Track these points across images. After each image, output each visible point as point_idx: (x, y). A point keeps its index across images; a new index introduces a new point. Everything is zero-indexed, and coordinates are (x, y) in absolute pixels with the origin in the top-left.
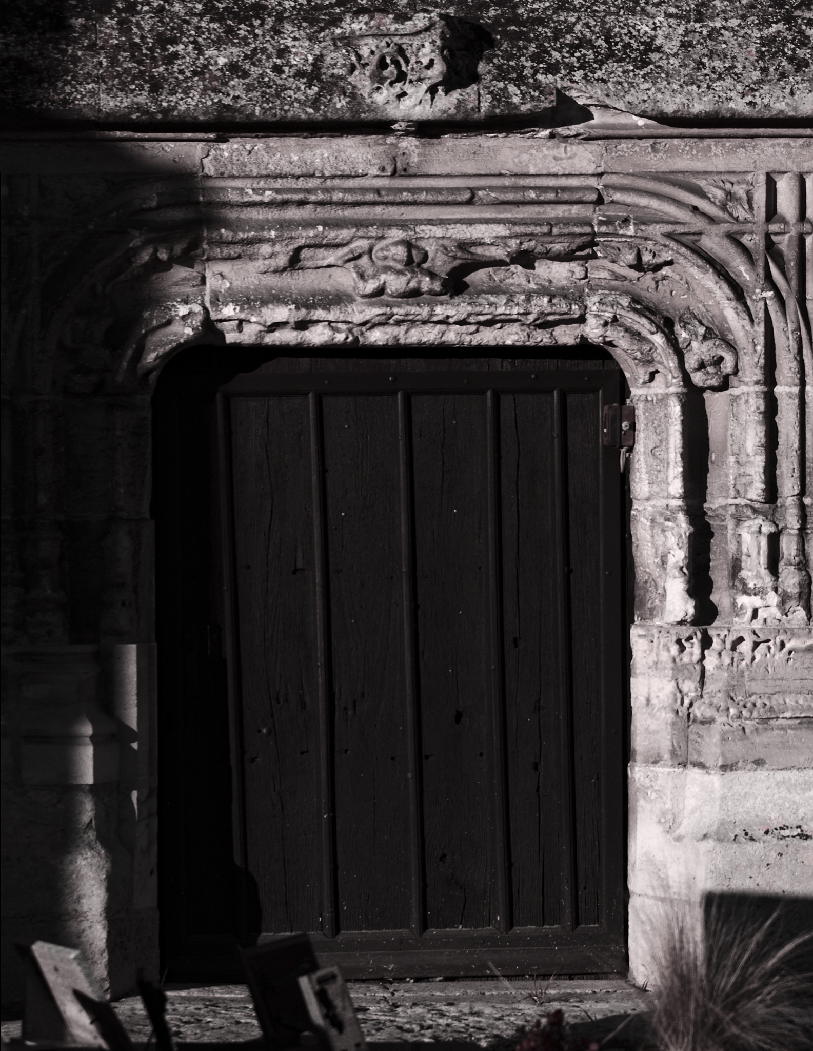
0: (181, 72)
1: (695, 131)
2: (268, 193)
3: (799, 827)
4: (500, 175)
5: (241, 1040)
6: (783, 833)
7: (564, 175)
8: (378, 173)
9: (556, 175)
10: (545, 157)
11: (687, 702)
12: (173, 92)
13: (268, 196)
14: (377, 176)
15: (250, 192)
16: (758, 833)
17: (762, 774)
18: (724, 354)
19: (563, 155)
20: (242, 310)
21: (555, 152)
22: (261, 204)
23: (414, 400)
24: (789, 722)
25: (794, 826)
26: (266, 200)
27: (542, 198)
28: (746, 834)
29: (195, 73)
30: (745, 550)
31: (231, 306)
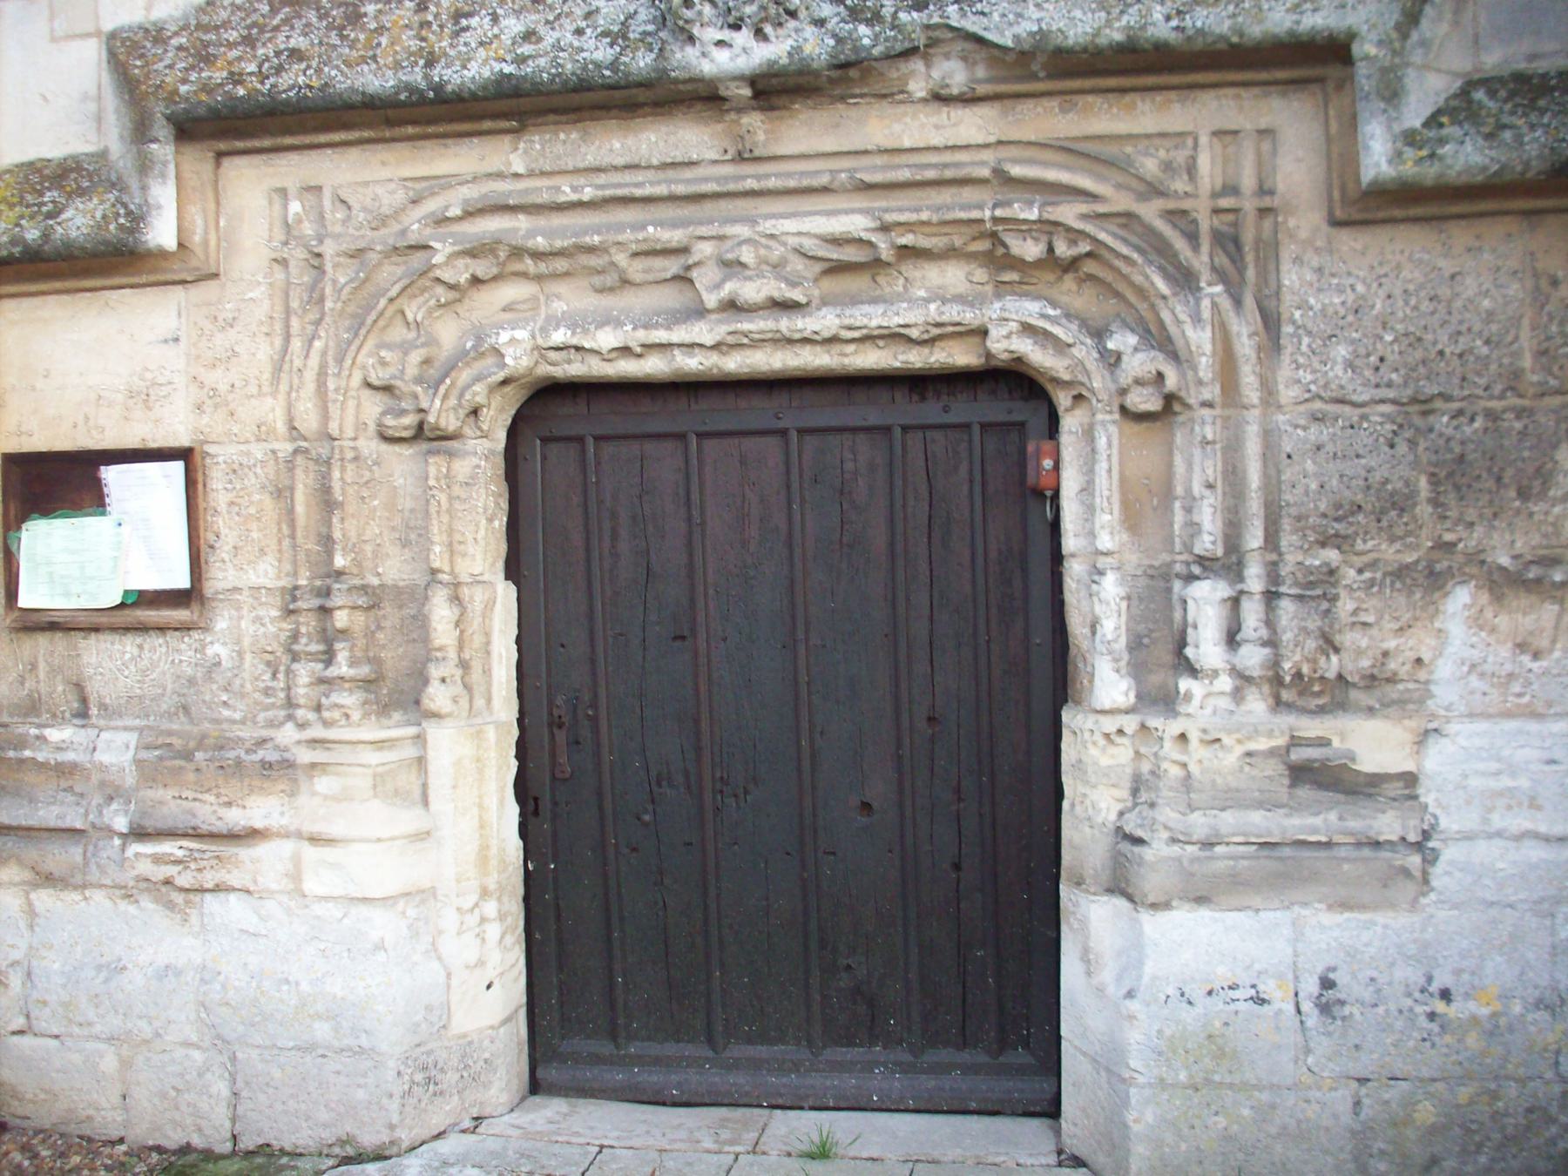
0: (466, 44)
1: (1112, 82)
2: (587, 190)
3: (1253, 986)
4: (866, 152)
5: (805, 1125)
6: (1232, 994)
7: (947, 148)
8: (716, 157)
9: (936, 149)
10: (923, 126)
11: (362, 1081)
12: (448, 66)
13: (588, 194)
14: (715, 162)
15: (568, 190)
16: (1197, 993)
17: (1204, 913)
18: (1162, 368)
19: (946, 122)
20: (574, 333)
21: (934, 120)
22: (580, 205)
23: (178, 467)
24: (1241, 848)
25: (1248, 984)
26: (586, 198)
27: (918, 177)
28: (1182, 995)
29: (481, 44)
30: (1190, 619)
31: (562, 330)
